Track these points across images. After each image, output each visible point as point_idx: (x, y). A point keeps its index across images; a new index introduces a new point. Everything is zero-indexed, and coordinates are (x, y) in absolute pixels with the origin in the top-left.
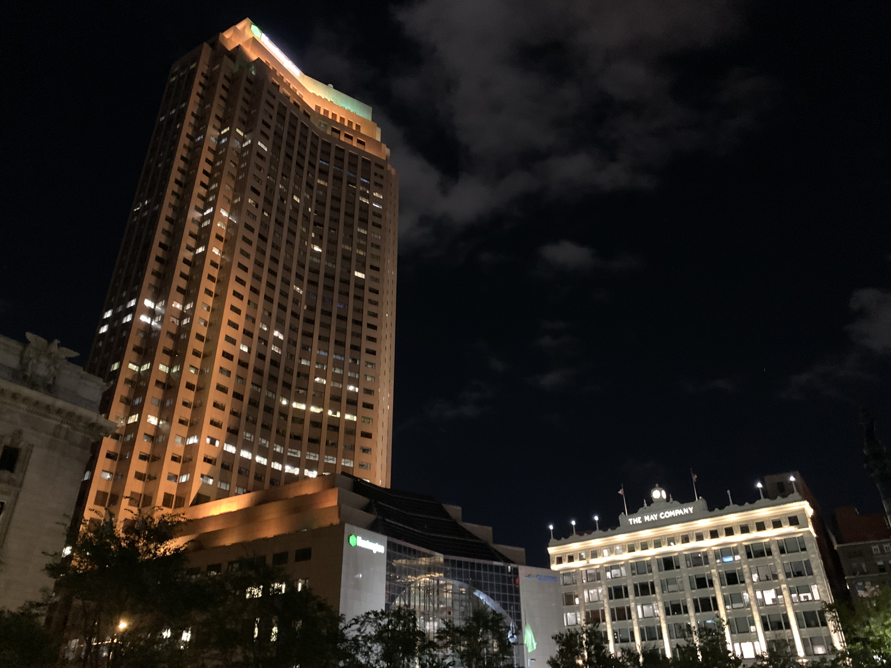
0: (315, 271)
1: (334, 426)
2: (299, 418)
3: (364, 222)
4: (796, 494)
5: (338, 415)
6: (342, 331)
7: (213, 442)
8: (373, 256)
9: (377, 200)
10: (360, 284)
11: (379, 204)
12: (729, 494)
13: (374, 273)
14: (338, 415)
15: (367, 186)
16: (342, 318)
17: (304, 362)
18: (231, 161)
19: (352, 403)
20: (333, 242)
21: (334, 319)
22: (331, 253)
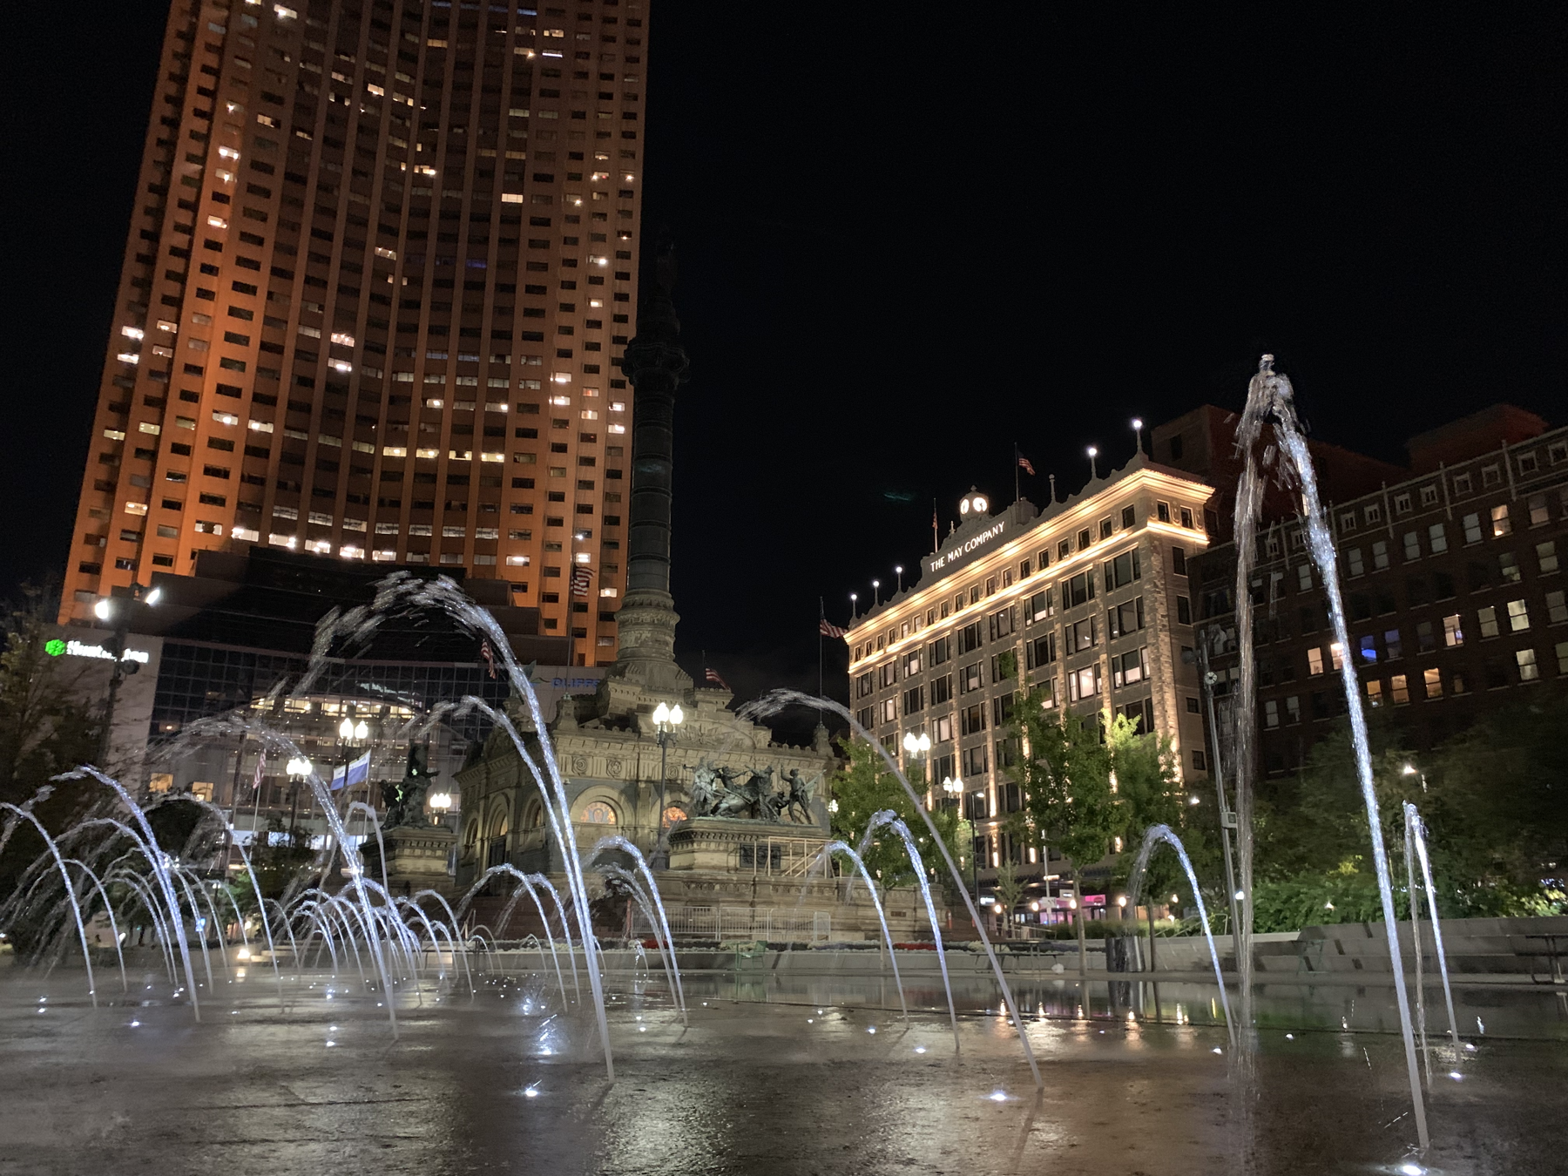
0: (421, 212)
1: (458, 476)
2: (393, 471)
3: (521, 96)
4: (1140, 456)
5: (468, 456)
6: (473, 309)
7: (209, 529)
8: (539, 156)
9: (553, 44)
10: (388, 234)
11: (556, 50)
12: (1052, 481)
13: (543, 188)
14: (468, 456)
15: (531, 22)
16: (474, 286)
17: (404, 378)
18: (237, 57)
19: (495, 434)
20: (457, 150)
21: (458, 291)
22: (451, 175)
